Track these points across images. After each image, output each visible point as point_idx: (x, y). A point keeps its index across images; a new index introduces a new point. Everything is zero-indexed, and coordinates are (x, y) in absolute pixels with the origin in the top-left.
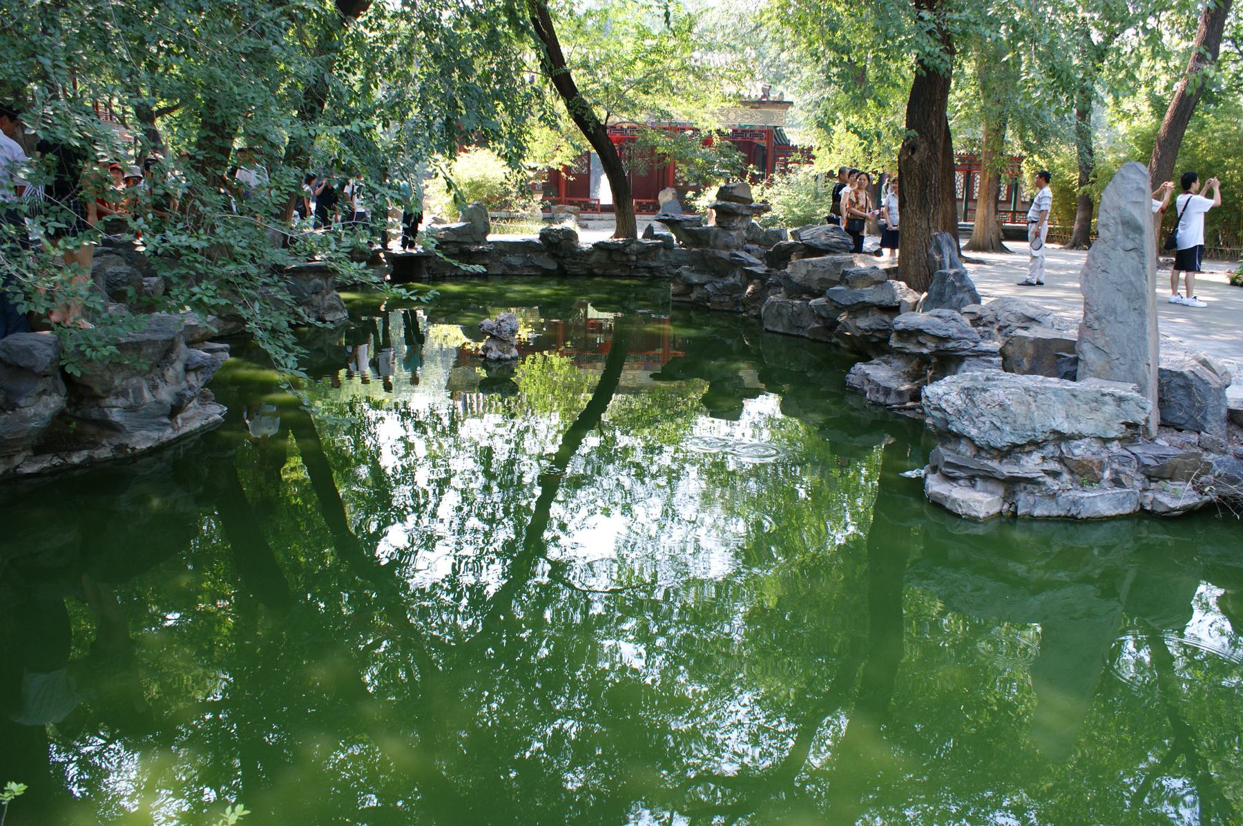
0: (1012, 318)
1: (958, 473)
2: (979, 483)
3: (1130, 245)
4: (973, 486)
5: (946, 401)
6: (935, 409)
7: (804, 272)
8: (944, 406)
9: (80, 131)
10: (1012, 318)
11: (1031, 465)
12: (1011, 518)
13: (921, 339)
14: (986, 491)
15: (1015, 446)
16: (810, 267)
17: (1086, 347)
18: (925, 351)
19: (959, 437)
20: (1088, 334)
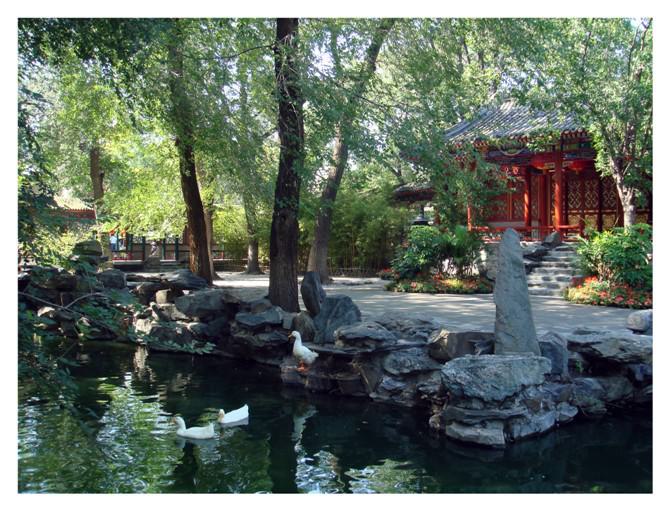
0: (411, 323)
1: (474, 421)
2: (488, 424)
3: (517, 275)
4: (484, 427)
5: (460, 378)
6: (454, 384)
7: (188, 305)
8: (459, 380)
9: (30, 146)
10: (411, 323)
11: (517, 408)
12: (511, 442)
13: (367, 343)
14: (493, 428)
15: (507, 397)
16: (192, 301)
17: (500, 335)
18: (369, 350)
19: (469, 399)
20: (501, 327)
